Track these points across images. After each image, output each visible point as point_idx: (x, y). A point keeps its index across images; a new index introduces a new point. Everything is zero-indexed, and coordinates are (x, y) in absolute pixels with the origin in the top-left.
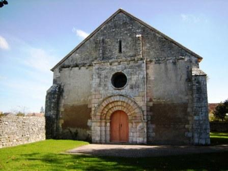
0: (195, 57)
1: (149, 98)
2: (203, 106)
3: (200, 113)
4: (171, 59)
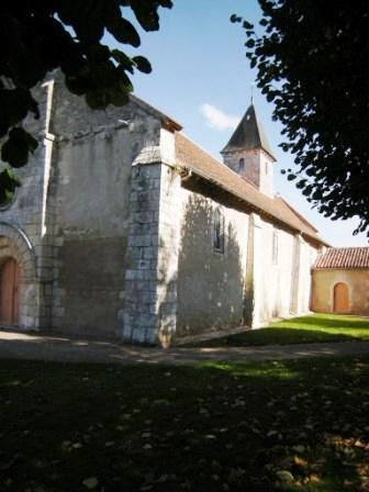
0: (155, 118)
1: (57, 227)
2: (147, 243)
3: (141, 261)
4: (103, 130)
